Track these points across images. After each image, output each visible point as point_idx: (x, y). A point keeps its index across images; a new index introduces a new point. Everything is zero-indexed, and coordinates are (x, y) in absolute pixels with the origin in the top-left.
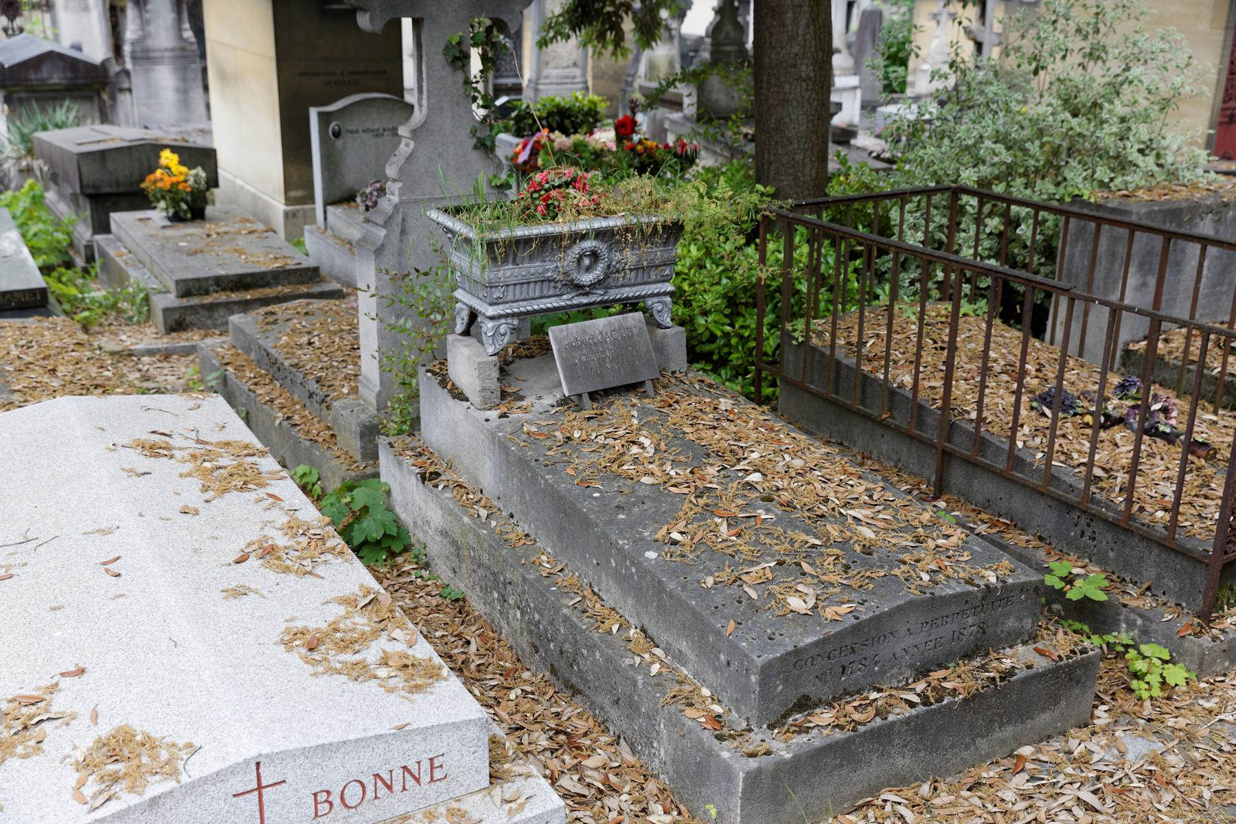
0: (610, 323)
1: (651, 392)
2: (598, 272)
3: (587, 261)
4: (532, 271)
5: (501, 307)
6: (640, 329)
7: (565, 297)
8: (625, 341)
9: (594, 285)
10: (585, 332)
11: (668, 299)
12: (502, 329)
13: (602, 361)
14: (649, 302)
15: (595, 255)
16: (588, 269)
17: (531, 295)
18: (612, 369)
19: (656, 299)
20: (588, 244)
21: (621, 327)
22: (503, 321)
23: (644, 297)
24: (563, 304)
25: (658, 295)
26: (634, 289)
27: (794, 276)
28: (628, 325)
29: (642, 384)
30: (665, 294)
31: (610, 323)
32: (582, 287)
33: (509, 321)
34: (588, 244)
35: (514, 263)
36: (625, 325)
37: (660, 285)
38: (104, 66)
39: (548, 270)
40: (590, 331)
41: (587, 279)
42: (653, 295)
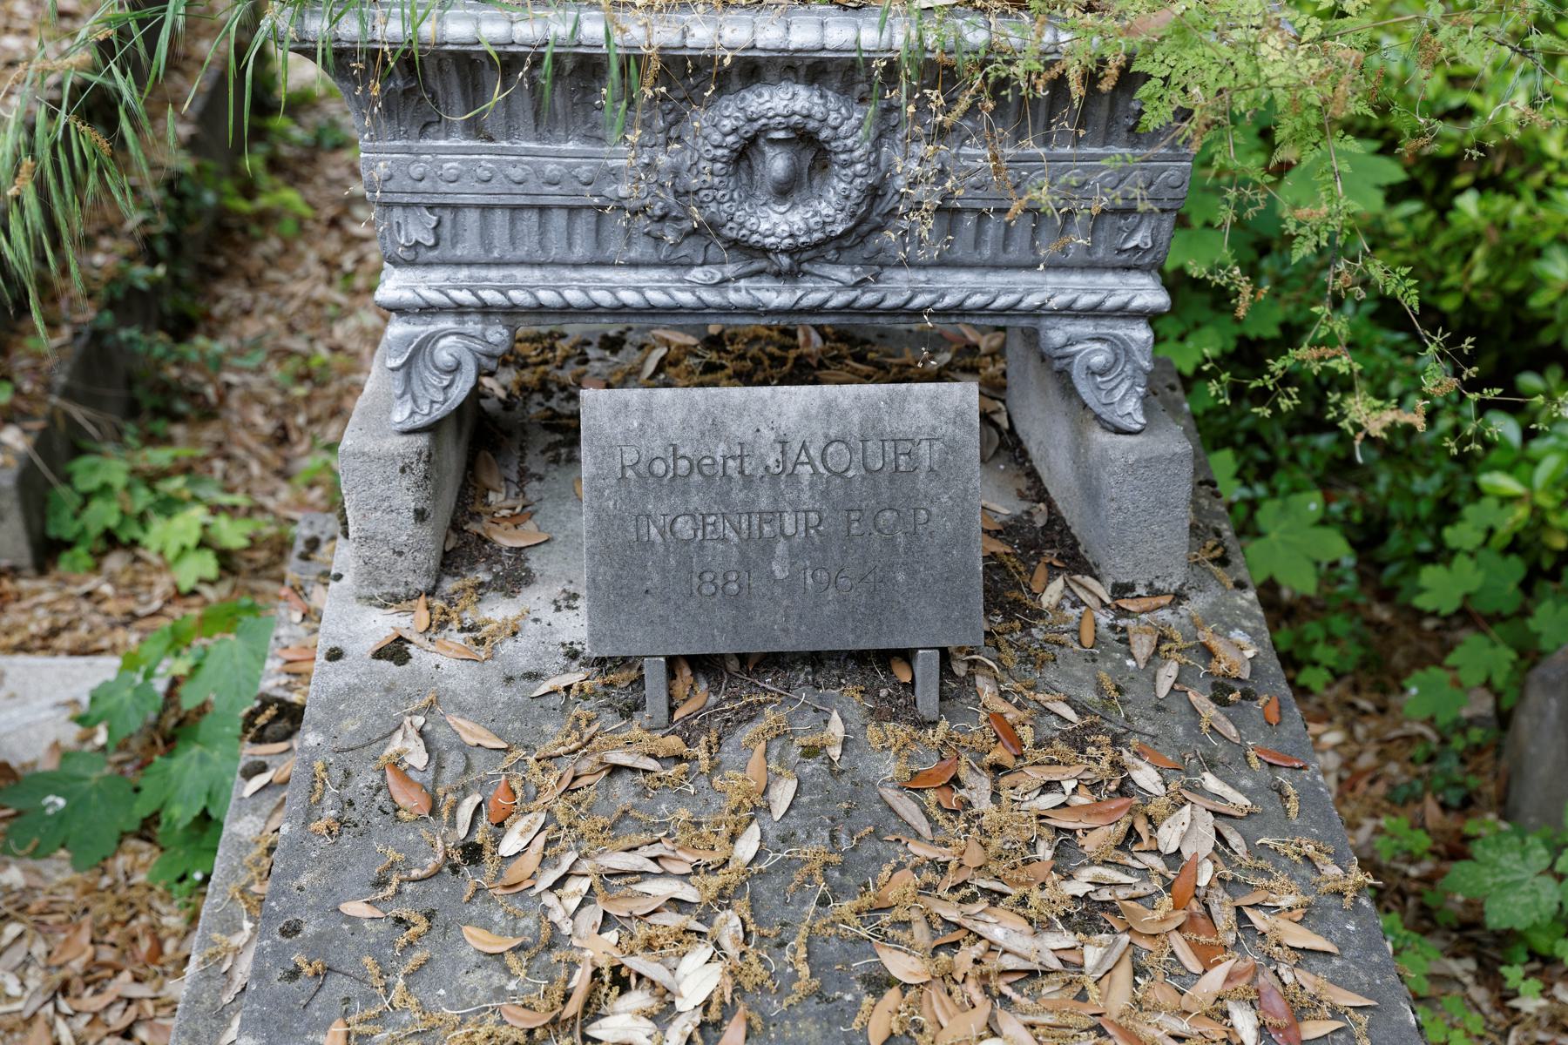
0: (829, 408)
1: (927, 700)
2: (827, 208)
3: (777, 163)
4: (551, 168)
5: (438, 275)
6: (952, 447)
7: (697, 274)
8: (879, 487)
9: (801, 258)
10: (716, 428)
11: (1141, 333)
12: (445, 351)
13: (758, 549)
14: (1056, 334)
15: (808, 143)
16: (785, 191)
17: (554, 253)
18: (790, 585)
19: (1085, 328)
20: (782, 101)
21: (871, 430)
22: (448, 323)
23: (1037, 312)
24: (686, 298)
25: (1094, 313)
26: (995, 280)
27: (1272, 369)
28: (904, 427)
29: (907, 656)
30: (1125, 313)
31: (829, 408)
32: (764, 251)
33: (472, 325)
34: (782, 101)
35: (475, 128)
36: (891, 425)
37: (1109, 279)
38: (124, 658)
39: (615, 175)
40: (739, 429)
41: (777, 223)
42: (1069, 312)
